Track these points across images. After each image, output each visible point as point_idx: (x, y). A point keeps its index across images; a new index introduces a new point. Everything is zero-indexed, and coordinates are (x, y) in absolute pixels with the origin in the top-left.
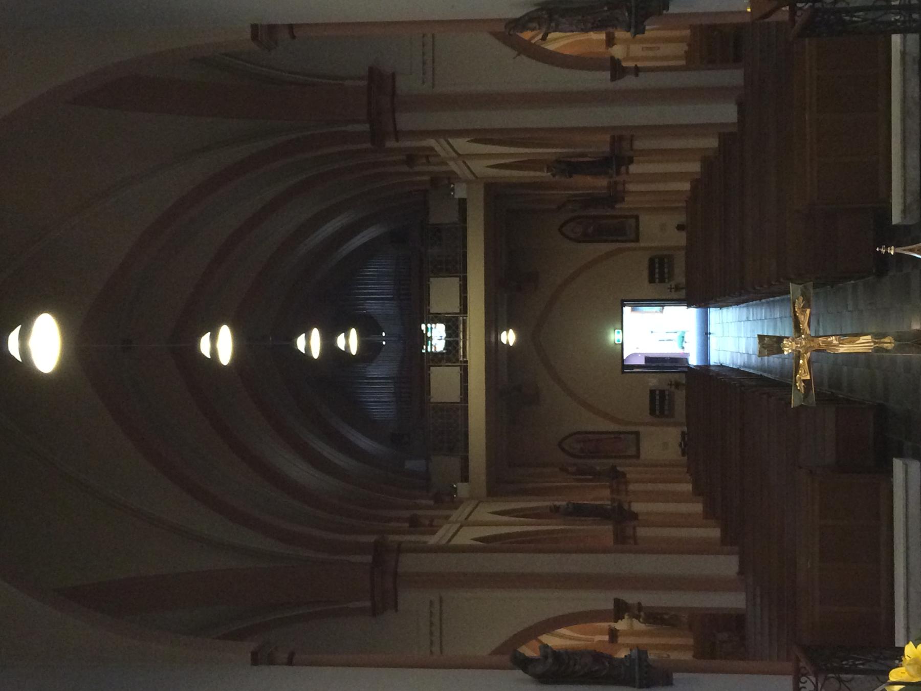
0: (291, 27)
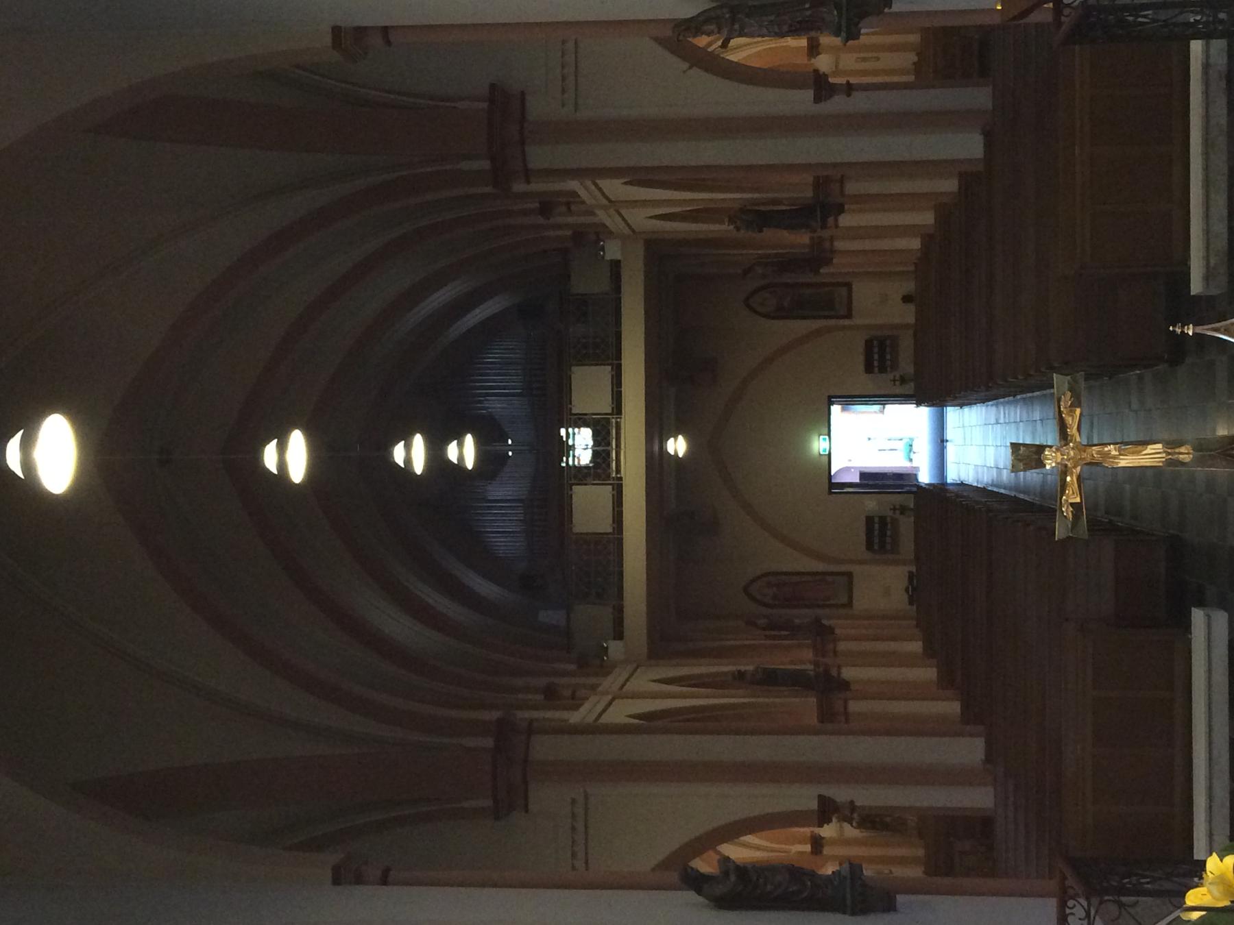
0: (385, 30)
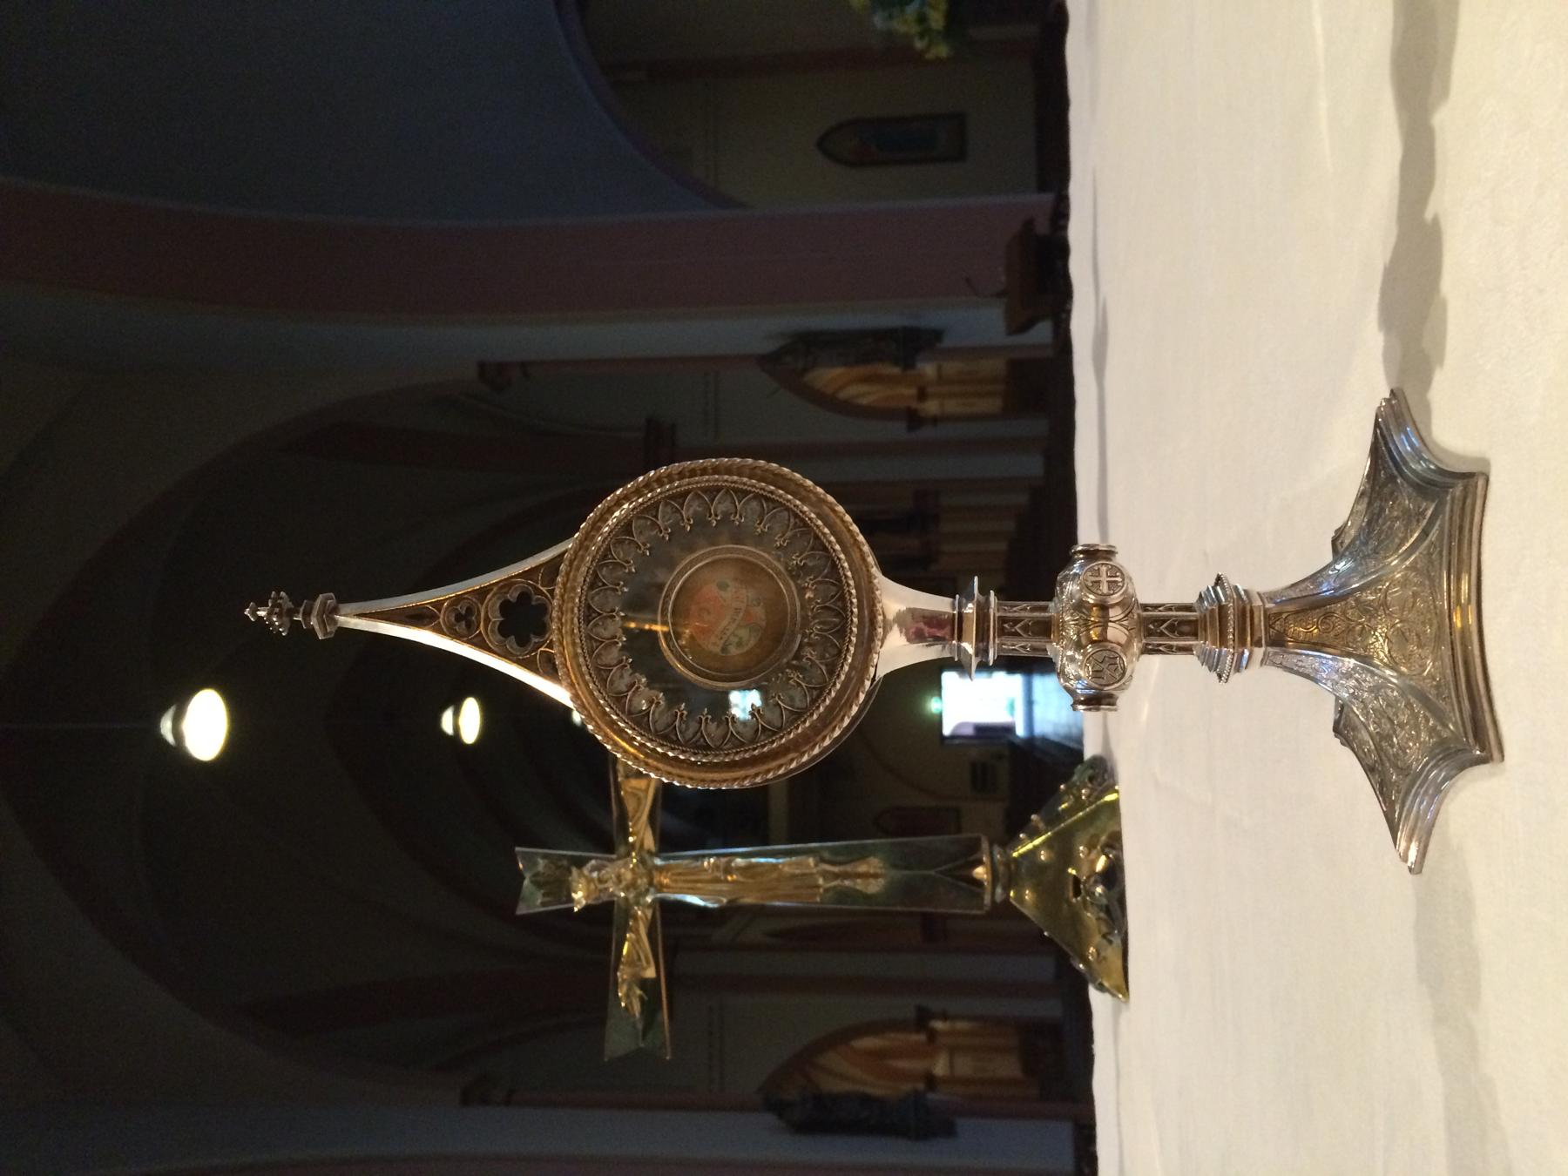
0: (524, 365)
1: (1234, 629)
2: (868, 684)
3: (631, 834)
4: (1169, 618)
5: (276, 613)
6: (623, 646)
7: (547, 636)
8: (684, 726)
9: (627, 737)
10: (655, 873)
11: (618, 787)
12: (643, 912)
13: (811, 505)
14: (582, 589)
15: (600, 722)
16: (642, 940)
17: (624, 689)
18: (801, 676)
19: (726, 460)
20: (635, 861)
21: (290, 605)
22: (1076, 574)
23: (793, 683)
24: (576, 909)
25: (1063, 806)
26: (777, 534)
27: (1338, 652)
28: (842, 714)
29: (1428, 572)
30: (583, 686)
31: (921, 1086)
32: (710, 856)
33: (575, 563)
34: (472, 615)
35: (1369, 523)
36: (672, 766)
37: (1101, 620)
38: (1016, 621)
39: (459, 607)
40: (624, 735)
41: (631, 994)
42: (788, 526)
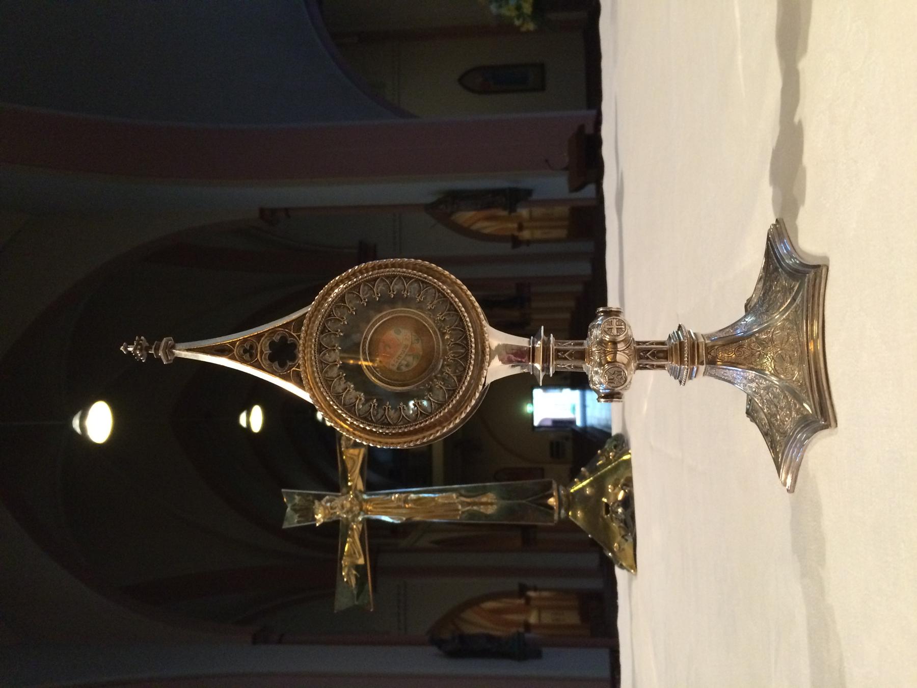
0: (286, 210)
1: (688, 355)
2: (481, 387)
3: (350, 481)
4: (651, 349)
5: (139, 349)
6: (340, 366)
7: (296, 361)
8: (375, 412)
9: (343, 418)
10: (364, 504)
11: (342, 454)
12: (357, 526)
13: (449, 285)
14: (316, 334)
15: (327, 410)
16: (356, 542)
17: (341, 391)
18: (442, 383)
19: (399, 259)
20: (352, 496)
21: (147, 344)
22: (599, 324)
23: (438, 387)
24: (317, 525)
25: (600, 463)
26: (429, 302)
27: (746, 367)
28: (466, 405)
29: (796, 321)
30: (317, 389)
31: (521, 630)
32: (396, 493)
33: (313, 319)
34: (253, 350)
35: (764, 294)
36: (368, 435)
37: (613, 350)
38: (565, 351)
39: (245, 345)
40: (341, 417)
41: (350, 573)
42: (435, 297)
